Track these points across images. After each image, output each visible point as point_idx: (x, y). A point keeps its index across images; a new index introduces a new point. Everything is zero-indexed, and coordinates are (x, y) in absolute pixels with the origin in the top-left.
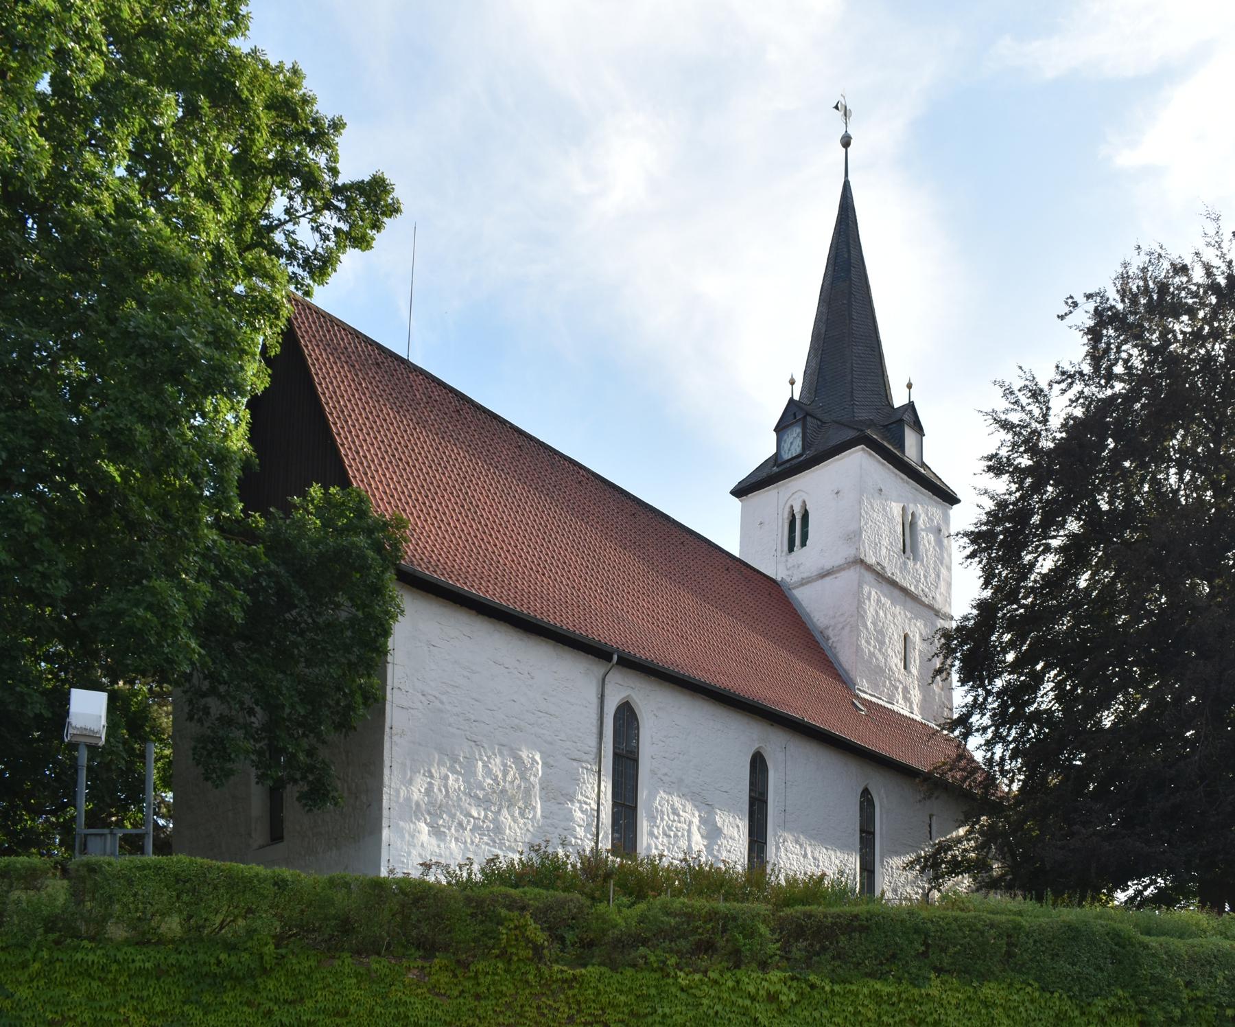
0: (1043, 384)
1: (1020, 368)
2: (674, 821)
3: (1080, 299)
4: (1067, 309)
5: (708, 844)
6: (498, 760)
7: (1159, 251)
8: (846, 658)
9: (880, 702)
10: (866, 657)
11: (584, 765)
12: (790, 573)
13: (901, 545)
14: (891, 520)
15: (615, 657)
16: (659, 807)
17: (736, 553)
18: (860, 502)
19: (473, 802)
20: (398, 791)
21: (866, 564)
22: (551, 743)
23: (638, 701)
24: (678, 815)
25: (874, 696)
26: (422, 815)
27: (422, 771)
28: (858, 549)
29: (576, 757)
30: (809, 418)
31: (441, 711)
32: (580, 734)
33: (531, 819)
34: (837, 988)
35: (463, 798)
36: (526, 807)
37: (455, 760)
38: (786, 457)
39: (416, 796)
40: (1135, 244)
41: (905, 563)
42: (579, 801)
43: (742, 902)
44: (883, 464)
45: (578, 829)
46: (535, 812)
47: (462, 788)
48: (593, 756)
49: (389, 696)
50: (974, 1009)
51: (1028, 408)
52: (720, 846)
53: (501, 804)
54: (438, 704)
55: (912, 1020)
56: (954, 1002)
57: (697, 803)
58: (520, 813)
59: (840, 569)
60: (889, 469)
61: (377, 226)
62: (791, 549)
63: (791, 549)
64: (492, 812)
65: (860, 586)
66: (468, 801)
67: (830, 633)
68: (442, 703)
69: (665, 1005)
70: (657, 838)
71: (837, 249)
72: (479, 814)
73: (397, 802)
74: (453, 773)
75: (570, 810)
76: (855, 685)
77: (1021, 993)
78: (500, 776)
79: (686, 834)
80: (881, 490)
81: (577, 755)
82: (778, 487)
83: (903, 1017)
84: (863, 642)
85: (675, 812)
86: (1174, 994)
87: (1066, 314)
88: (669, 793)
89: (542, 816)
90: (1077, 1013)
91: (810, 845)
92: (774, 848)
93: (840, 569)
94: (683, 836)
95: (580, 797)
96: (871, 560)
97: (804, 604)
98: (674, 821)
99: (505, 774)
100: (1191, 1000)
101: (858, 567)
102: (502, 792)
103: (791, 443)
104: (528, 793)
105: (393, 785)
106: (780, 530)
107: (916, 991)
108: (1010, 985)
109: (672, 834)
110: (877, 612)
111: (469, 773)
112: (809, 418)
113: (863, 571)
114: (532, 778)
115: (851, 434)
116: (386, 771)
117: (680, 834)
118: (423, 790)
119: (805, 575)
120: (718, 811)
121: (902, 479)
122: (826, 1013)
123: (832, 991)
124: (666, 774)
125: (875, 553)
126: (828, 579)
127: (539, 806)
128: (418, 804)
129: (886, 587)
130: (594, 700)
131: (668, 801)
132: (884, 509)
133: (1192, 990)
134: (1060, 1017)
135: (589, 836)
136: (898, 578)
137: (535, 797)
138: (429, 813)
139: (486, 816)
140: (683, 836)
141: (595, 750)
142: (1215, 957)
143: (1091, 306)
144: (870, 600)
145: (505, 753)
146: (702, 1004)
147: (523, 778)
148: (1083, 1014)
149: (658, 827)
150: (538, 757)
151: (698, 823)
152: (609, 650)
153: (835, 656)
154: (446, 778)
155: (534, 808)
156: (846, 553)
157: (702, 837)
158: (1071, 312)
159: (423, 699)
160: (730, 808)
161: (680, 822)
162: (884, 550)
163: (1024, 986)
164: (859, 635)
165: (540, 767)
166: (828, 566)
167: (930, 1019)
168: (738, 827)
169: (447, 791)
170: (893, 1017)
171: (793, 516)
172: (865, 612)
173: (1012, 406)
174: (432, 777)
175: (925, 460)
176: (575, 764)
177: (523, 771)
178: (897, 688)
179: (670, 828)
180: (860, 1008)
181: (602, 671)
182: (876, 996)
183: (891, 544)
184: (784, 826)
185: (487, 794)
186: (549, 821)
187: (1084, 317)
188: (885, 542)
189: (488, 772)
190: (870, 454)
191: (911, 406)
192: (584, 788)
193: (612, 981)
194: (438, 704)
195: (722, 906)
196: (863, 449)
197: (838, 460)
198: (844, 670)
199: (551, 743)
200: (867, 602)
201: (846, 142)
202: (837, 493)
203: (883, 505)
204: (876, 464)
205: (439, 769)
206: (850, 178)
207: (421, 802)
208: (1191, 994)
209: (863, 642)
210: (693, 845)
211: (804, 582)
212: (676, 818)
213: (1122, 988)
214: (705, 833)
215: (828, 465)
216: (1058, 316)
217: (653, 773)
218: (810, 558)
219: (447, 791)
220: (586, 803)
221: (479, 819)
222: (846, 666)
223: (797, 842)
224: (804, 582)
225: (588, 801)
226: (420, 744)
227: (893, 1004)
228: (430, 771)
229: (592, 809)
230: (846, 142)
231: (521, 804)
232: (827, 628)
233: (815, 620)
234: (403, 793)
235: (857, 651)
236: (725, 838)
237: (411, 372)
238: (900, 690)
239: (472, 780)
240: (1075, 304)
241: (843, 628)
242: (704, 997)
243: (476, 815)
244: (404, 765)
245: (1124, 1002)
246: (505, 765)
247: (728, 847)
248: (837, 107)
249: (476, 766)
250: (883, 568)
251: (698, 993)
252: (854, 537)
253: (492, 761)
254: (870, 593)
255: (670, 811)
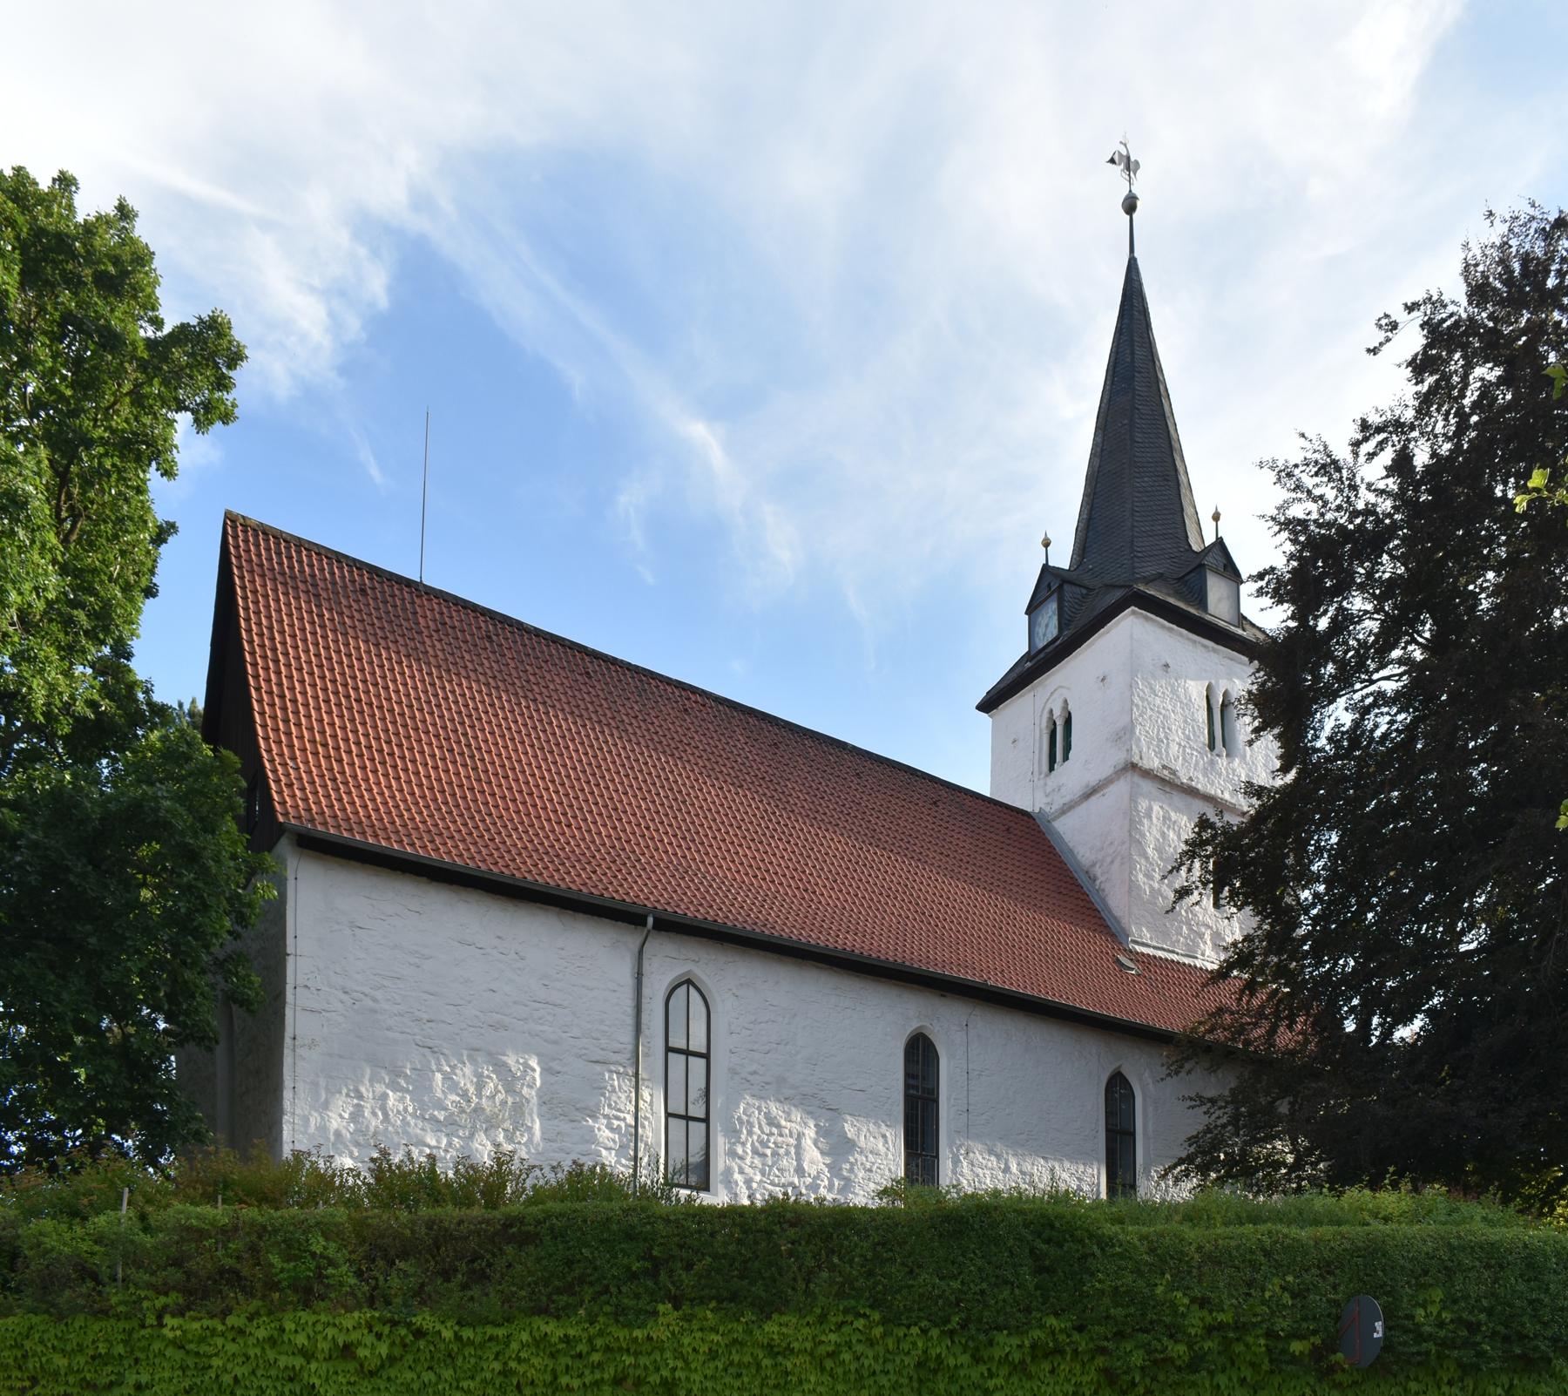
0: (1342, 453)
1: (1303, 435)
2: (772, 1134)
3: (1399, 315)
4: (1381, 336)
5: (833, 1162)
6: (468, 1070)
7: (1532, 211)
8: (1117, 902)
9: (1175, 957)
10: (1146, 897)
11: (613, 1068)
12: (1049, 800)
13: (1205, 738)
14: (1188, 704)
15: (650, 920)
16: (745, 1118)
17: (986, 792)
18: (1131, 686)
19: (428, 1127)
20: (306, 1120)
21: (1140, 768)
22: (555, 1042)
23: (704, 978)
24: (779, 1126)
25: (1173, 952)
26: (346, 1147)
27: (344, 1091)
28: (1129, 750)
29: (599, 1058)
30: (1066, 587)
31: (375, 1012)
32: (606, 1028)
33: (525, 1144)
34: (467, 1333)
35: (412, 1122)
36: (516, 1128)
37: (397, 1072)
38: (1040, 645)
39: (335, 1124)
40: (1484, 211)
41: (1212, 763)
42: (606, 1117)
43: (197, 1205)
44: (1170, 630)
45: (604, 1153)
46: (531, 1135)
47: (410, 1109)
48: (628, 1056)
49: (289, 997)
50: (747, 1359)
51: (1317, 492)
52: (852, 1164)
53: (474, 1127)
54: (370, 1003)
55: (618, 1381)
56: (704, 1348)
57: (810, 1109)
58: (506, 1137)
59: (1108, 782)
60: (1181, 635)
61: (222, 383)
62: (1051, 769)
63: (1051, 769)
64: (459, 1137)
65: (1133, 800)
66: (420, 1124)
67: (1098, 871)
68: (375, 1000)
69: (141, 1370)
70: (741, 1158)
71: (1117, 353)
72: (438, 1141)
73: (305, 1133)
74: (395, 1090)
75: (592, 1129)
76: (1128, 936)
77: (846, 1329)
78: (472, 1090)
79: (793, 1150)
80: (1167, 666)
81: (600, 1055)
82: (1033, 689)
83: (598, 1376)
84: (1141, 876)
85: (772, 1122)
86: (1168, 1320)
87: (1381, 344)
88: (761, 1098)
89: (543, 1139)
90: (965, 1359)
91: (1015, 1155)
92: (949, 1164)
93: (1108, 782)
94: (788, 1153)
95: (607, 1110)
96: (1152, 762)
97: (1067, 838)
98: (772, 1134)
99: (480, 1087)
100: (1210, 1330)
101: (1129, 775)
102: (475, 1110)
103: (1047, 626)
104: (519, 1109)
105: (298, 1111)
106: (1037, 745)
107: (622, 1334)
108: (822, 1319)
109: (768, 1152)
110: (1163, 834)
111: (421, 1089)
112: (1066, 587)
113: (1137, 779)
114: (525, 1091)
115: (1118, 594)
116: (287, 1095)
117: (782, 1151)
118: (346, 1116)
119: (1066, 800)
120: (848, 1117)
121: (1205, 646)
122: (447, 1374)
123: (458, 1337)
124: (755, 1073)
125: (1158, 753)
126: (1093, 799)
127: (537, 1126)
128: (338, 1134)
129: (1178, 798)
130: (628, 980)
131: (759, 1109)
132: (1174, 692)
133: (1211, 1312)
134: (928, 1368)
135: (623, 1161)
136: (1201, 784)
137: (531, 1115)
138: (357, 1144)
139: (450, 1144)
140: (788, 1153)
141: (630, 1047)
142: (1267, 1254)
143: (1418, 317)
144: (1150, 818)
145: (479, 1059)
146: (210, 1367)
147: (510, 1089)
148: (977, 1360)
149: (743, 1144)
150: (534, 1063)
151: (813, 1135)
152: (640, 911)
153: (1104, 901)
154: (385, 1097)
155: (530, 1129)
156: (1117, 757)
157: (822, 1153)
158: (1388, 340)
159: (344, 997)
160: (865, 1113)
161: (781, 1135)
162: (1174, 748)
163: (849, 1318)
164: (1132, 869)
165: (537, 1075)
166: (1093, 783)
167: (654, 1379)
168: (884, 1136)
169: (386, 1114)
170: (581, 1376)
171: (1055, 723)
172: (1143, 835)
173: (1293, 495)
174: (360, 1097)
175: (1244, 611)
176: (598, 1068)
177: (510, 1082)
178: (1201, 936)
179: (764, 1144)
180: (513, 1364)
181: (635, 948)
182: (540, 1342)
183: (1189, 738)
184: (968, 1132)
185: (452, 1114)
186: (555, 1145)
187: (1412, 340)
188: (1177, 737)
189: (453, 1086)
190: (1147, 618)
191: (1220, 543)
192: (614, 1098)
193: (46, 1337)
194: (369, 1003)
195: (250, 1213)
196: (1134, 613)
197: (1103, 634)
198: (1115, 918)
199: (555, 1042)
200: (1145, 821)
201: (1130, 206)
202: (1103, 680)
203: (1172, 686)
204: (1159, 631)
205: (372, 1086)
206: (1136, 255)
207: (344, 1132)
208: (1209, 1319)
209: (1141, 876)
210: (805, 1166)
211: (1066, 809)
212: (775, 1130)
213: (1056, 1315)
214: (825, 1147)
215: (1093, 644)
216: (1369, 351)
217: (733, 1072)
218: (1074, 774)
219: (386, 1114)
220: (618, 1118)
221: (439, 1148)
222: (1117, 912)
223: (991, 1152)
224: (1066, 809)
225: (622, 1115)
226: (341, 1057)
227: (580, 1356)
228: (357, 1091)
229: (628, 1126)
230: (1130, 206)
231: (507, 1125)
232: (1094, 865)
233: (1079, 857)
234: (314, 1120)
235: (1130, 890)
236: (861, 1153)
237: (419, 596)
238: (1207, 937)
239: (426, 1098)
240: (1394, 326)
241: (1112, 862)
242: (216, 1355)
243: (433, 1143)
244: (315, 1085)
245: (1062, 1337)
246: (479, 1076)
247: (868, 1165)
248: (1112, 161)
249: (431, 1080)
250: (1174, 772)
251: (204, 1348)
252: (1124, 734)
253: (458, 1071)
254: (1150, 809)
255: (764, 1122)
